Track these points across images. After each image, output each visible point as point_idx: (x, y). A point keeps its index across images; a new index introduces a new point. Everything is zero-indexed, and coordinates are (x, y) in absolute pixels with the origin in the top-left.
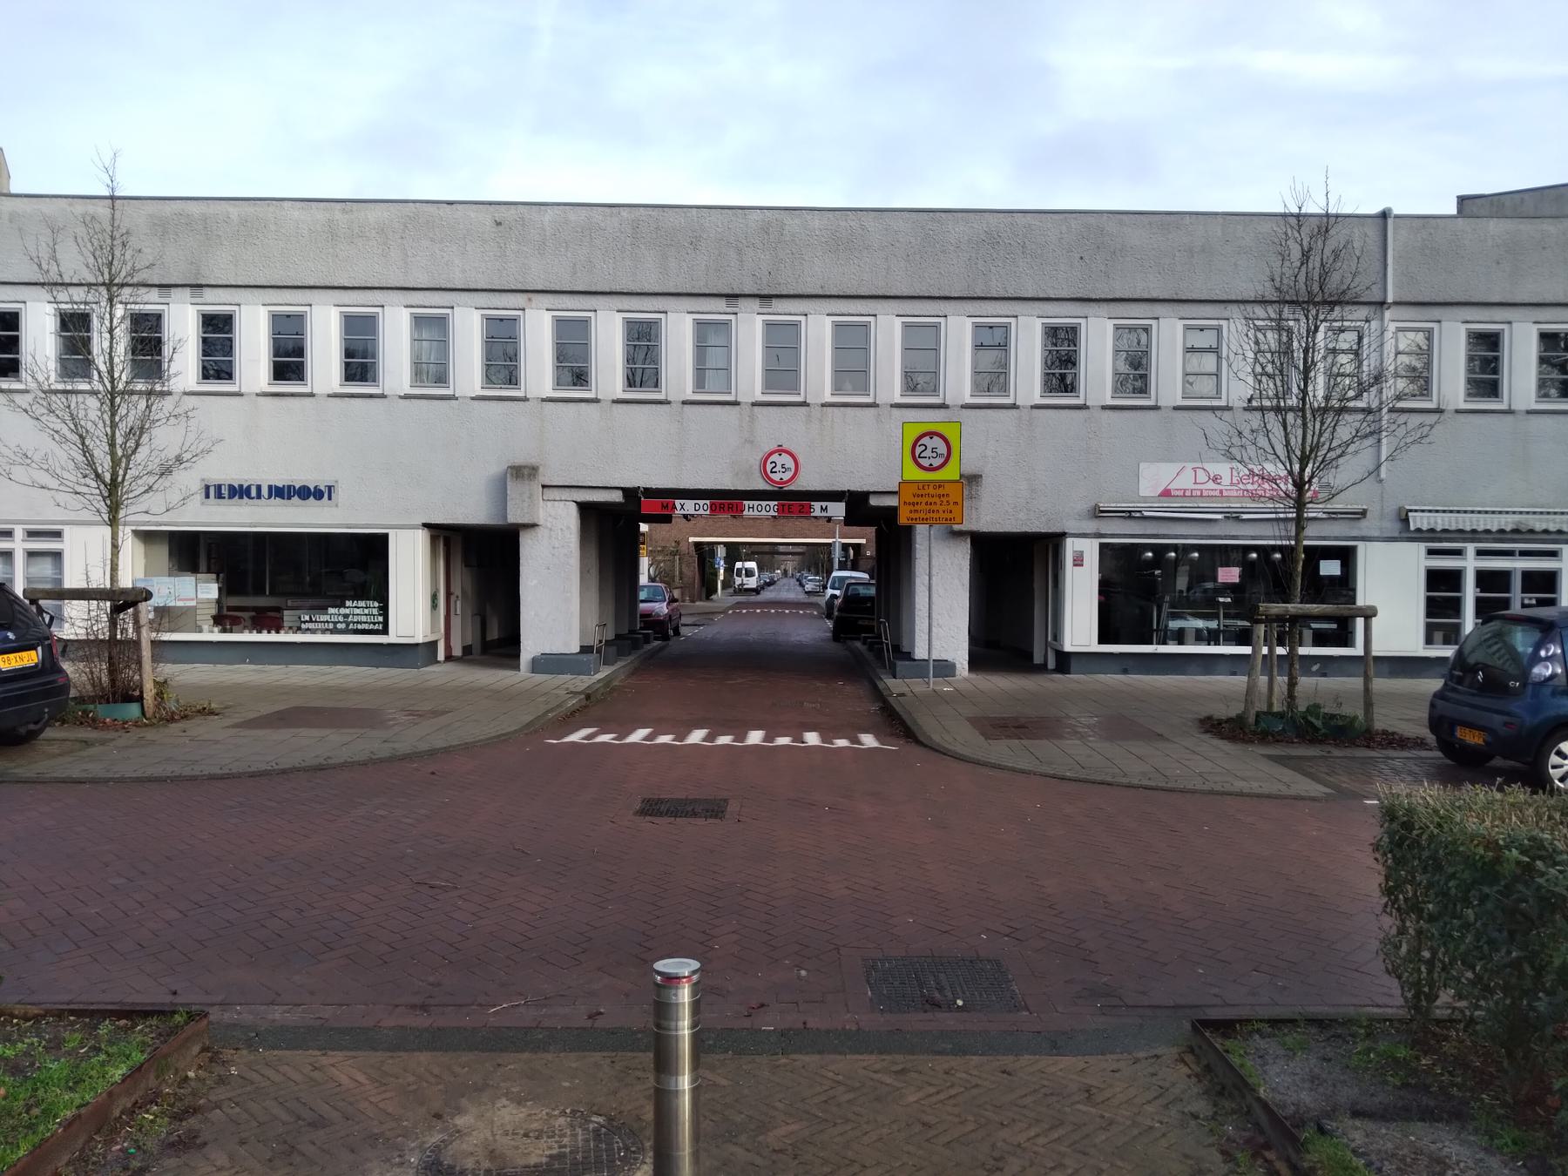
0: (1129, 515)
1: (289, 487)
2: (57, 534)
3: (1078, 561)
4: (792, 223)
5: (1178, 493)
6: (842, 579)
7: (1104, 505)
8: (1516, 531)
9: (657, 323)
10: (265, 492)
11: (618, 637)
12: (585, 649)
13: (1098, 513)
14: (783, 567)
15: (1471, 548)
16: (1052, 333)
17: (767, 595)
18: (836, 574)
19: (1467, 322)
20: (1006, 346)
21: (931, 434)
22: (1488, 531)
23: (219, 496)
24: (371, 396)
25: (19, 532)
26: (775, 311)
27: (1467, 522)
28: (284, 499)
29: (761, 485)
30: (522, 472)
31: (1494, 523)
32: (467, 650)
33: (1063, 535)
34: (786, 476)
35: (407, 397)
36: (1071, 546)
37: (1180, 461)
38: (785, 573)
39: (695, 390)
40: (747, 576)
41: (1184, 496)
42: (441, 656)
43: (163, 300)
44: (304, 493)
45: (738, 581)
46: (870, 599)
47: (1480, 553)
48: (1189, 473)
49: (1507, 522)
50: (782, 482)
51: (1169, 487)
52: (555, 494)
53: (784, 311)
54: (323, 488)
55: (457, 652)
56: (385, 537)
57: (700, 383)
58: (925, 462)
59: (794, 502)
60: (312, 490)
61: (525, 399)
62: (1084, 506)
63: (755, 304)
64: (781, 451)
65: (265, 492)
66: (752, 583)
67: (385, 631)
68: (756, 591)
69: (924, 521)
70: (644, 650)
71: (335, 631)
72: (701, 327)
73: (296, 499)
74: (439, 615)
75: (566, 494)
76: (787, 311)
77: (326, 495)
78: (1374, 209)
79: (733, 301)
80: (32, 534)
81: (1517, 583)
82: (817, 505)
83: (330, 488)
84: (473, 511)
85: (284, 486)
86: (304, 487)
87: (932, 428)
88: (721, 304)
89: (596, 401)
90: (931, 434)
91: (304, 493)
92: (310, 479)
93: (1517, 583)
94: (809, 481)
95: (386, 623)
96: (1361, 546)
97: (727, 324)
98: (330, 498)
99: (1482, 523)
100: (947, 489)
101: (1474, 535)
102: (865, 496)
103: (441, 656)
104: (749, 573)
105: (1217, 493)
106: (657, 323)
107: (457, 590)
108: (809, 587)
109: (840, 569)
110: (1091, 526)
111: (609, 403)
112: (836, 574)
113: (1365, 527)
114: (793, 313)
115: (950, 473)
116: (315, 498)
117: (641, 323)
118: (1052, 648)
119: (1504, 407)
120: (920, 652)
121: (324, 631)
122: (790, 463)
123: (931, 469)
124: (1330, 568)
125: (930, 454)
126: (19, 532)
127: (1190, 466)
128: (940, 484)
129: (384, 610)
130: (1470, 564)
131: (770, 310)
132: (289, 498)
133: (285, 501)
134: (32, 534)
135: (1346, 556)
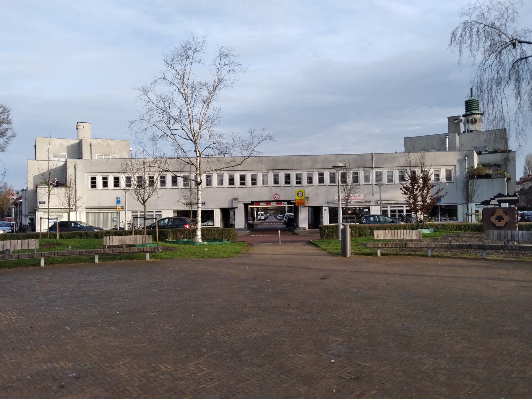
0: (333, 203)
2: (161, 212)
3: (325, 210)
4: (277, 158)
6: (288, 215)
7: (329, 202)
8: (396, 203)
9: (256, 175)
10: (194, 204)
13: (328, 203)
14: (269, 213)
15: (389, 206)
16: (320, 174)
17: (267, 220)
18: (286, 214)
21: (300, 192)
22: (391, 204)
23: (187, 205)
25: (139, 212)
27: (388, 202)
29: (273, 200)
30: (235, 199)
31: (392, 202)
33: (323, 206)
34: (278, 198)
35: (216, 188)
36: (324, 208)
38: (270, 214)
40: (262, 216)
45: (259, 217)
46: (293, 218)
47: (390, 207)
49: (394, 202)
50: (277, 199)
52: (240, 202)
53: (276, 172)
56: (213, 211)
58: (299, 196)
59: (279, 202)
61: (235, 187)
62: (326, 202)
63: (272, 171)
64: (276, 194)
65: (194, 204)
66: (263, 217)
67: (214, 225)
68: (264, 220)
69: (299, 205)
71: (206, 226)
72: (263, 175)
75: (242, 202)
78: (371, 153)
80: (156, 212)
81: (397, 212)
82: (283, 203)
84: (226, 206)
87: (300, 191)
88: (266, 171)
89: (247, 187)
90: (300, 192)
93: (397, 212)
94: (281, 199)
95: (214, 224)
97: (267, 174)
99: (390, 202)
100: (303, 200)
101: (389, 204)
102: (291, 201)
104: (262, 215)
106: (256, 175)
108: (279, 218)
109: (287, 213)
110: (327, 205)
112: (286, 214)
113: (371, 204)
115: (303, 198)
117: (253, 175)
119: (394, 183)
120: (300, 226)
121: (205, 226)
122: (278, 196)
123: (300, 197)
124: (366, 210)
126: (139, 212)
128: (302, 199)
129: (214, 222)
130: (389, 209)
134: (156, 212)
135: (369, 208)
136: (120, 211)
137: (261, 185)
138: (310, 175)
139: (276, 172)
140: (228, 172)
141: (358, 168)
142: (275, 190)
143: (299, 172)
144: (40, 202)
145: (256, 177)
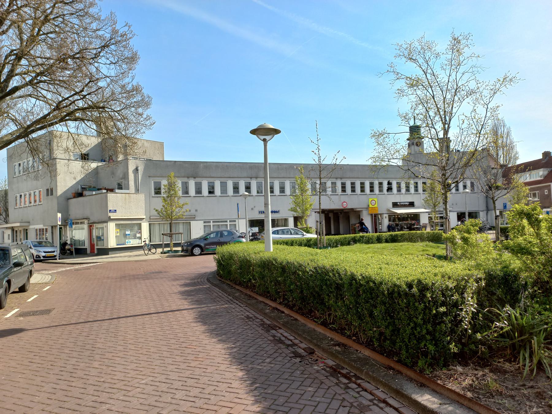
3: (386, 218)
4: (257, 165)
25: (228, 221)
35: (194, 197)
53: (198, 180)
64: (344, 202)
88: (335, 179)
126: (228, 221)
136: (191, 222)
137: (220, 194)
138: (211, 185)
139: (343, 181)
140: (369, 179)
141: (337, 178)
142: (344, 198)
143: (236, 180)
144: (110, 211)
145: (238, 185)
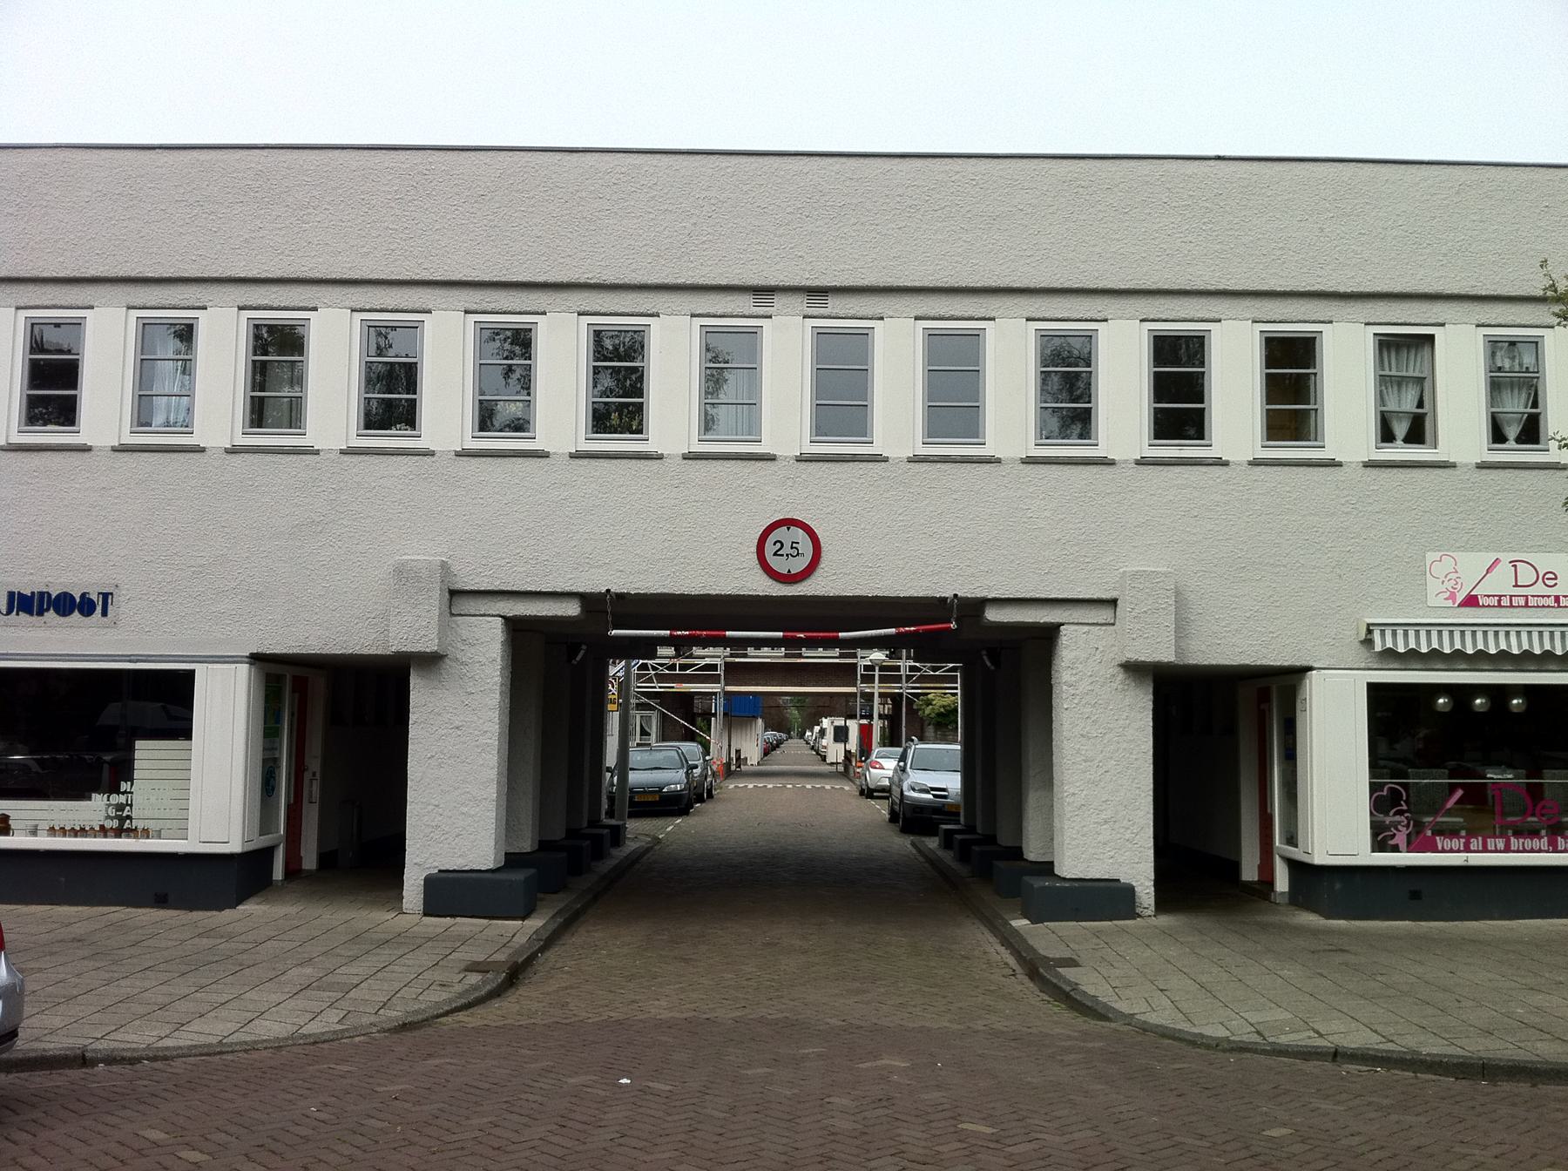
1: (42, 594)
5: (1486, 601)
11: (544, 846)
12: (512, 861)
19: (1483, 325)
20: (142, 360)
24: (854, 458)
26: (834, 312)
28: (32, 614)
32: (327, 861)
37: (1487, 549)
39: (814, 438)
41: (1500, 606)
42: (278, 873)
43: (761, 311)
44: (65, 604)
48: (1505, 569)
51: (1472, 593)
53: (842, 315)
54: (94, 597)
55: (309, 861)
57: (142, 420)
60: (78, 600)
63: (800, 303)
70: (614, 862)
73: (51, 615)
74: (278, 808)
76: (851, 312)
77: (99, 609)
79: (765, 298)
83: (106, 596)
85: (33, 593)
86: (65, 594)
88: (745, 303)
91: (65, 604)
92: (76, 583)
96: (199, 669)
98: (105, 613)
103: (278, 873)
105: (1551, 602)
107: (314, 765)
111: (335, 456)
114: (148, 305)
116: (82, 612)
118: (1282, 857)
125: (791, 551)
127: (1506, 557)
131: (822, 311)
132: (41, 613)
133: (35, 618)
